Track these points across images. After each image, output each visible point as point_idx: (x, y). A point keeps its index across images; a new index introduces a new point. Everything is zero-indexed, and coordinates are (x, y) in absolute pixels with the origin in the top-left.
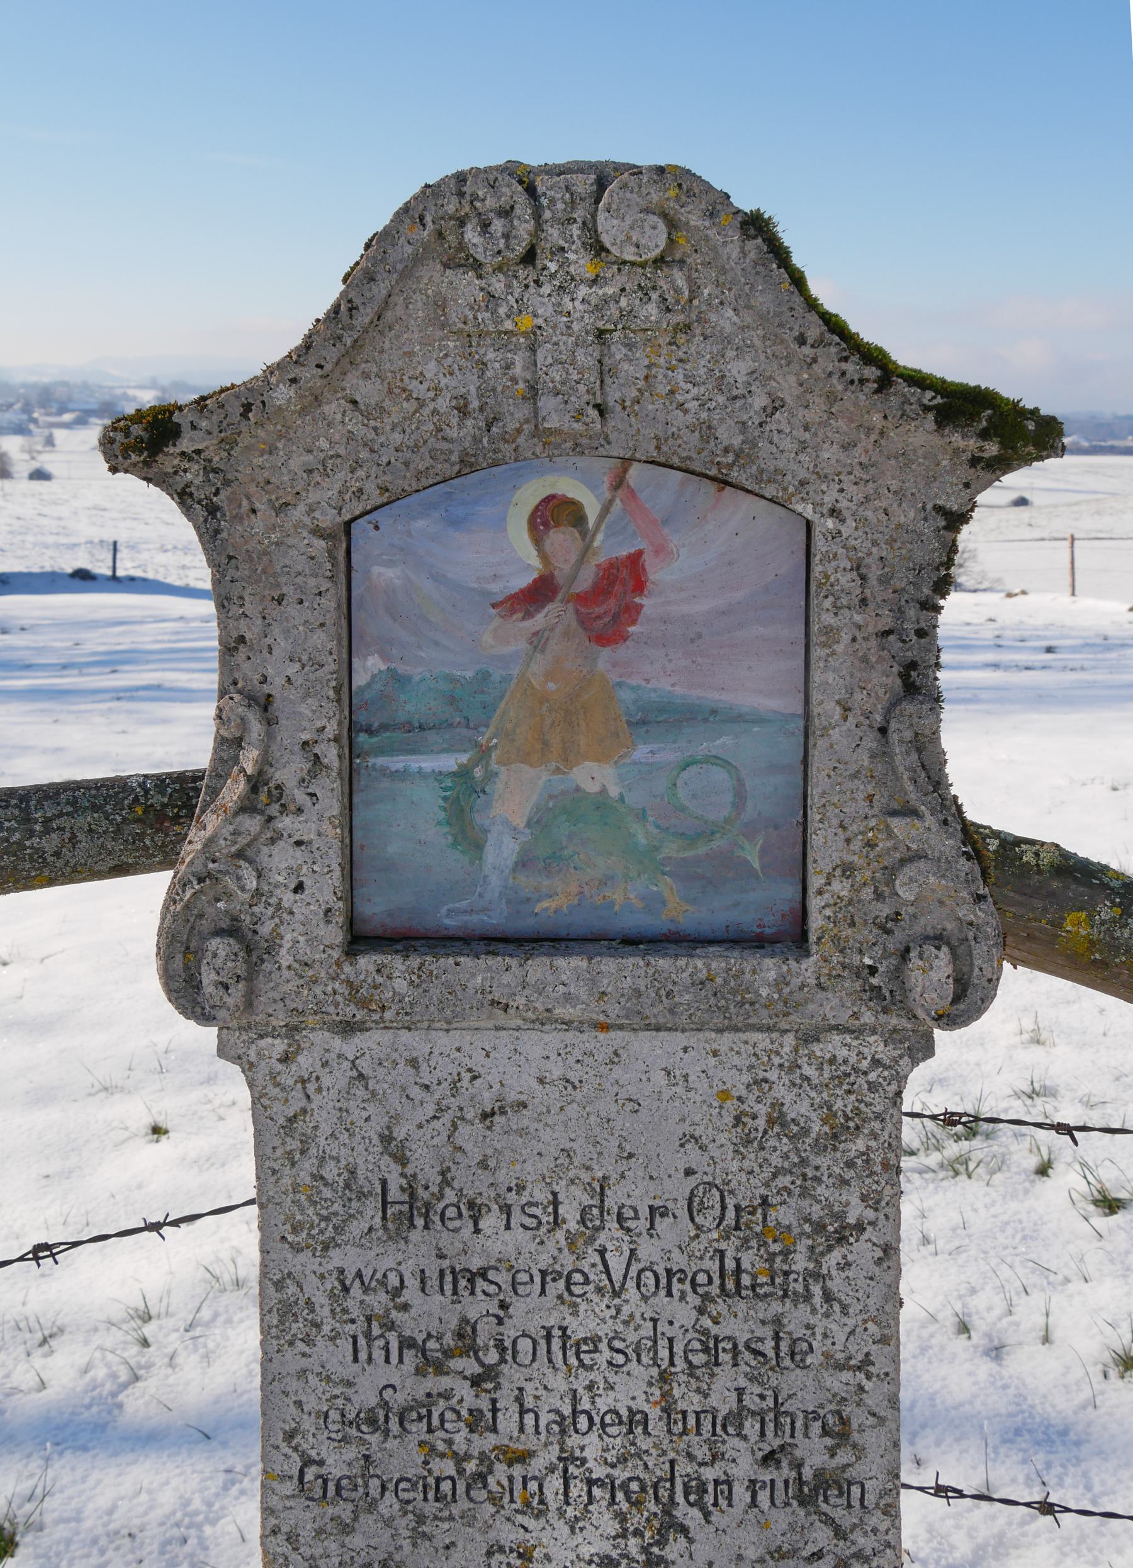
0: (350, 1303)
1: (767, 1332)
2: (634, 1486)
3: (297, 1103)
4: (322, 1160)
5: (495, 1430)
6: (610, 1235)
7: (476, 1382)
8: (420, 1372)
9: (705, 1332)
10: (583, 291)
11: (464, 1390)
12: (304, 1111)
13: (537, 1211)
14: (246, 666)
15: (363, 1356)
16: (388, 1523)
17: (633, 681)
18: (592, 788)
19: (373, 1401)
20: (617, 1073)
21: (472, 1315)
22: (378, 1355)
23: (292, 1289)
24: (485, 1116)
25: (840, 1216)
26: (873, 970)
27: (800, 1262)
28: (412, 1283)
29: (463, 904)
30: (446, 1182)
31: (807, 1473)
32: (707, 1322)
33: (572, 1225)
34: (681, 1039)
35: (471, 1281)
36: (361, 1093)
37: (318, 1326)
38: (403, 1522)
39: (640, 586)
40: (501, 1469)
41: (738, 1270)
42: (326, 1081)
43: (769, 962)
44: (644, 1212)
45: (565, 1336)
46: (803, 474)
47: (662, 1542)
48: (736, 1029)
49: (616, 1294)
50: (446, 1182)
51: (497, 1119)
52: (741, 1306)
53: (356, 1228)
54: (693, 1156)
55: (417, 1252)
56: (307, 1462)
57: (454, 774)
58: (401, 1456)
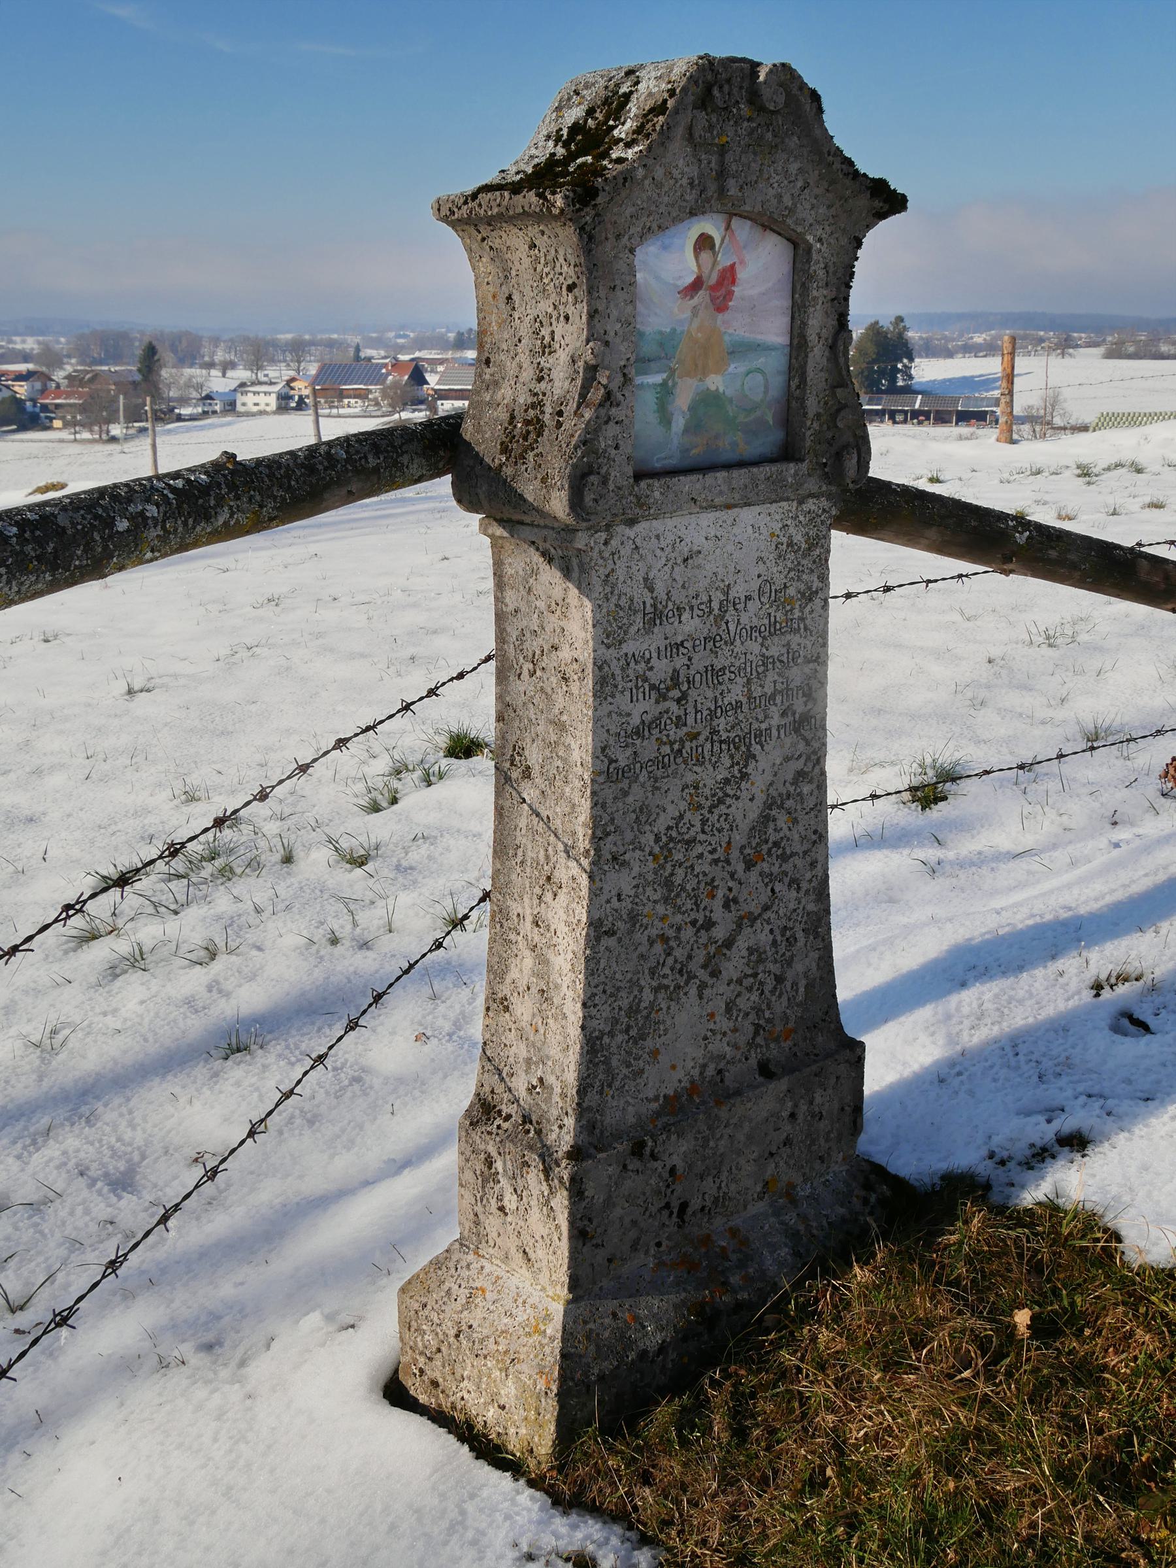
0: (630, 672)
1: (784, 650)
2: (737, 740)
3: (610, 566)
4: (620, 596)
5: (685, 725)
6: (730, 615)
7: (678, 701)
8: (657, 702)
9: (763, 656)
10: (745, 124)
11: (674, 707)
12: (613, 570)
13: (703, 607)
14: (598, 325)
15: (635, 698)
16: (643, 786)
17: (731, 331)
18: (713, 388)
19: (639, 721)
20: (736, 530)
21: (678, 667)
22: (641, 696)
23: (607, 668)
24: (685, 560)
25: (810, 588)
26: (825, 465)
27: (797, 614)
28: (655, 655)
29: (663, 455)
30: (669, 599)
31: (797, 716)
32: (764, 650)
33: (716, 612)
34: (757, 509)
35: (678, 649)
36: (636, 557)
37: (616, 687)
38: (648, 784)
39: (733, 282)
40: (688, 744)
41: (776, 622)
42: (622, 553)
43: (792, 465)
44: (743, 599)
45: (713, 670)
46: (811, 221)
47: (746, 766)
48: (775, 501)
49: (732, 644)
50: (669, 599)
51: (690, 561)
52: (776, 639)
53: (633, 629)
54: (761, 568)
55: (656, 640)
56: (611, 761)
57: (661, 385)
58: (648, 748)
